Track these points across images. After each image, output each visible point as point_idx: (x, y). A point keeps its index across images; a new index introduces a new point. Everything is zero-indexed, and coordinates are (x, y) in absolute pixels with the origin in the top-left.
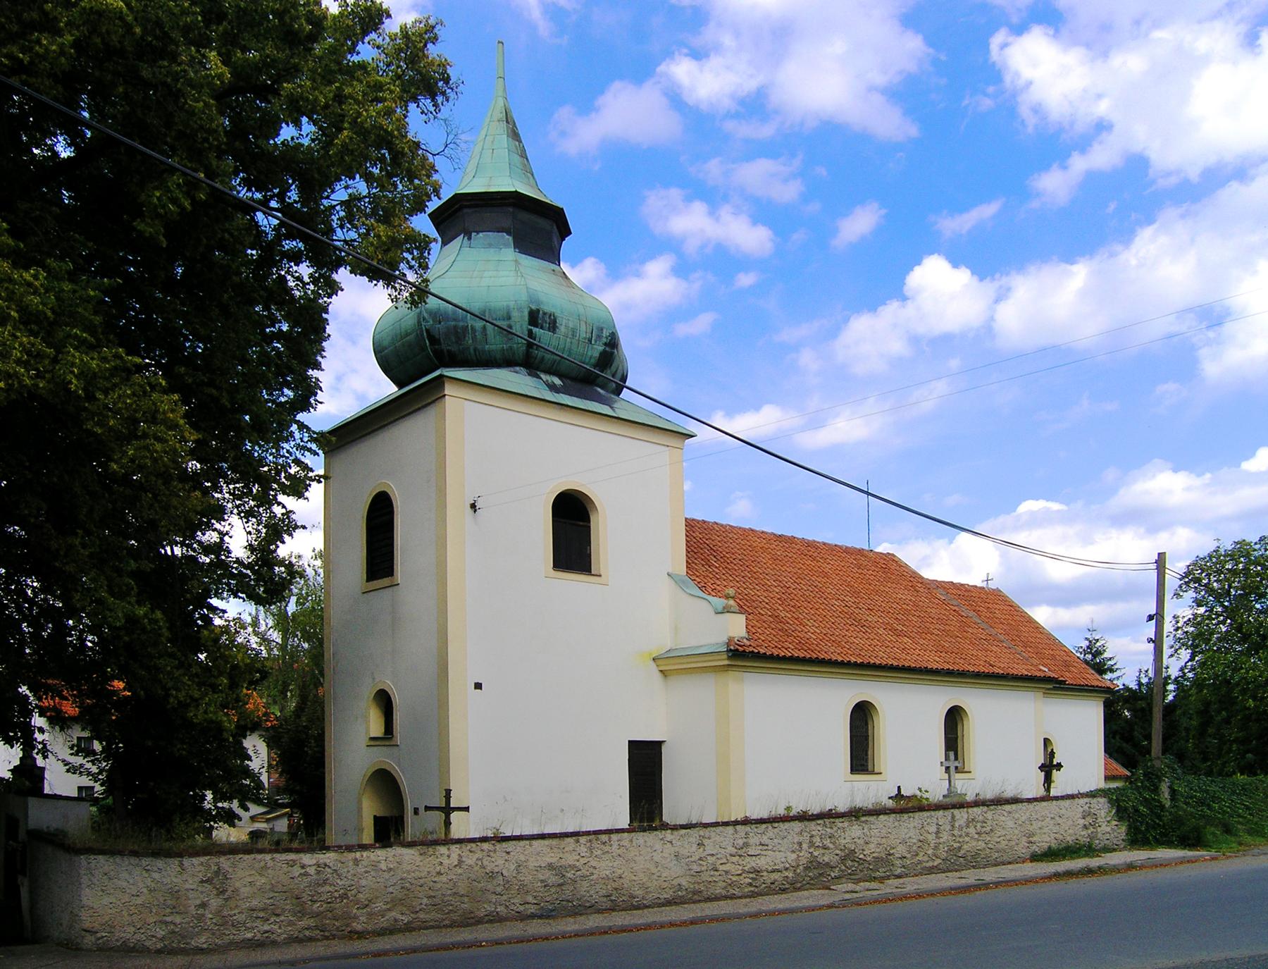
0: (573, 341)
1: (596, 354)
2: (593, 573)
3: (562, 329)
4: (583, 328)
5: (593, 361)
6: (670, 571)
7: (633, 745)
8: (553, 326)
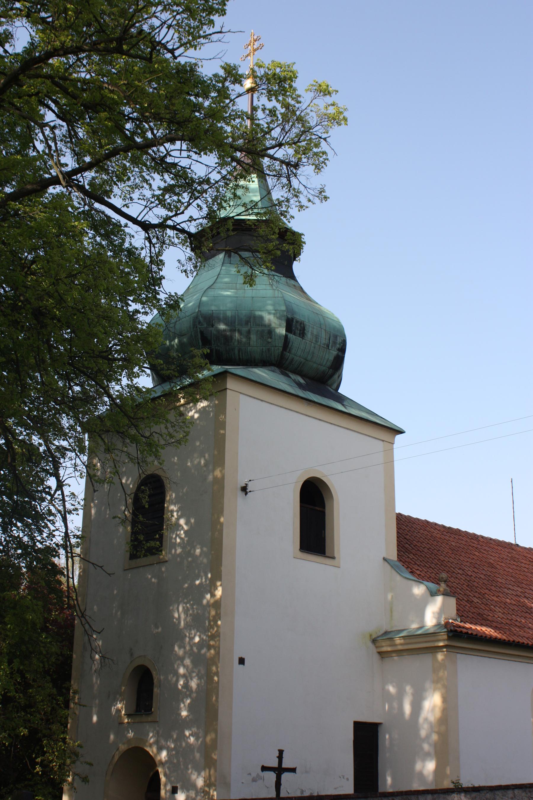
0: (316, 345)
1: (332, 358)
2: (327, 554)
3: (309, 336)
4: (323, 335)
5: (329, 364)
6: (385, 556)
7: (357, 725)
8: (302, 333)
